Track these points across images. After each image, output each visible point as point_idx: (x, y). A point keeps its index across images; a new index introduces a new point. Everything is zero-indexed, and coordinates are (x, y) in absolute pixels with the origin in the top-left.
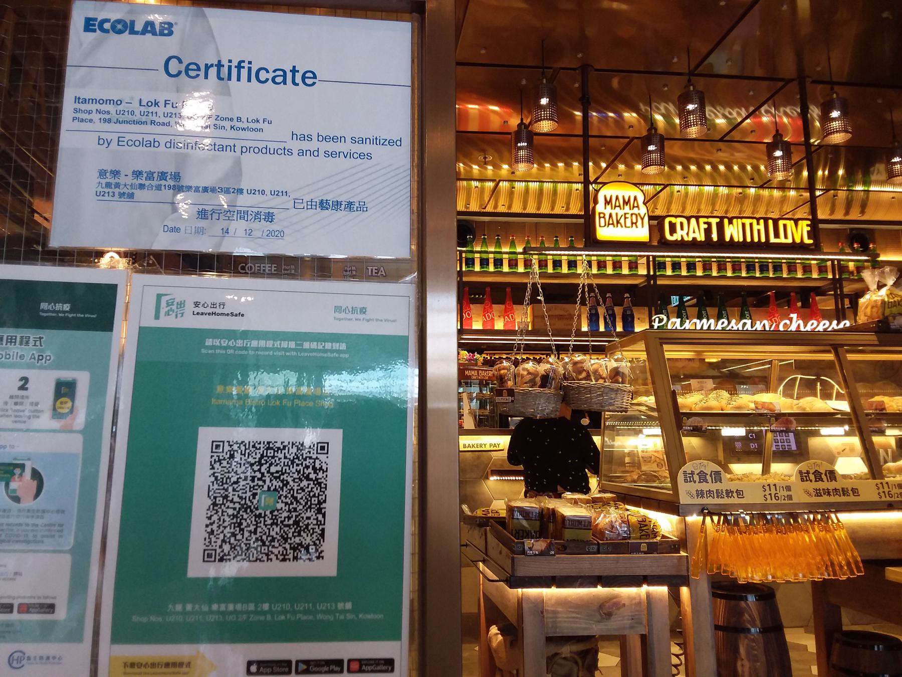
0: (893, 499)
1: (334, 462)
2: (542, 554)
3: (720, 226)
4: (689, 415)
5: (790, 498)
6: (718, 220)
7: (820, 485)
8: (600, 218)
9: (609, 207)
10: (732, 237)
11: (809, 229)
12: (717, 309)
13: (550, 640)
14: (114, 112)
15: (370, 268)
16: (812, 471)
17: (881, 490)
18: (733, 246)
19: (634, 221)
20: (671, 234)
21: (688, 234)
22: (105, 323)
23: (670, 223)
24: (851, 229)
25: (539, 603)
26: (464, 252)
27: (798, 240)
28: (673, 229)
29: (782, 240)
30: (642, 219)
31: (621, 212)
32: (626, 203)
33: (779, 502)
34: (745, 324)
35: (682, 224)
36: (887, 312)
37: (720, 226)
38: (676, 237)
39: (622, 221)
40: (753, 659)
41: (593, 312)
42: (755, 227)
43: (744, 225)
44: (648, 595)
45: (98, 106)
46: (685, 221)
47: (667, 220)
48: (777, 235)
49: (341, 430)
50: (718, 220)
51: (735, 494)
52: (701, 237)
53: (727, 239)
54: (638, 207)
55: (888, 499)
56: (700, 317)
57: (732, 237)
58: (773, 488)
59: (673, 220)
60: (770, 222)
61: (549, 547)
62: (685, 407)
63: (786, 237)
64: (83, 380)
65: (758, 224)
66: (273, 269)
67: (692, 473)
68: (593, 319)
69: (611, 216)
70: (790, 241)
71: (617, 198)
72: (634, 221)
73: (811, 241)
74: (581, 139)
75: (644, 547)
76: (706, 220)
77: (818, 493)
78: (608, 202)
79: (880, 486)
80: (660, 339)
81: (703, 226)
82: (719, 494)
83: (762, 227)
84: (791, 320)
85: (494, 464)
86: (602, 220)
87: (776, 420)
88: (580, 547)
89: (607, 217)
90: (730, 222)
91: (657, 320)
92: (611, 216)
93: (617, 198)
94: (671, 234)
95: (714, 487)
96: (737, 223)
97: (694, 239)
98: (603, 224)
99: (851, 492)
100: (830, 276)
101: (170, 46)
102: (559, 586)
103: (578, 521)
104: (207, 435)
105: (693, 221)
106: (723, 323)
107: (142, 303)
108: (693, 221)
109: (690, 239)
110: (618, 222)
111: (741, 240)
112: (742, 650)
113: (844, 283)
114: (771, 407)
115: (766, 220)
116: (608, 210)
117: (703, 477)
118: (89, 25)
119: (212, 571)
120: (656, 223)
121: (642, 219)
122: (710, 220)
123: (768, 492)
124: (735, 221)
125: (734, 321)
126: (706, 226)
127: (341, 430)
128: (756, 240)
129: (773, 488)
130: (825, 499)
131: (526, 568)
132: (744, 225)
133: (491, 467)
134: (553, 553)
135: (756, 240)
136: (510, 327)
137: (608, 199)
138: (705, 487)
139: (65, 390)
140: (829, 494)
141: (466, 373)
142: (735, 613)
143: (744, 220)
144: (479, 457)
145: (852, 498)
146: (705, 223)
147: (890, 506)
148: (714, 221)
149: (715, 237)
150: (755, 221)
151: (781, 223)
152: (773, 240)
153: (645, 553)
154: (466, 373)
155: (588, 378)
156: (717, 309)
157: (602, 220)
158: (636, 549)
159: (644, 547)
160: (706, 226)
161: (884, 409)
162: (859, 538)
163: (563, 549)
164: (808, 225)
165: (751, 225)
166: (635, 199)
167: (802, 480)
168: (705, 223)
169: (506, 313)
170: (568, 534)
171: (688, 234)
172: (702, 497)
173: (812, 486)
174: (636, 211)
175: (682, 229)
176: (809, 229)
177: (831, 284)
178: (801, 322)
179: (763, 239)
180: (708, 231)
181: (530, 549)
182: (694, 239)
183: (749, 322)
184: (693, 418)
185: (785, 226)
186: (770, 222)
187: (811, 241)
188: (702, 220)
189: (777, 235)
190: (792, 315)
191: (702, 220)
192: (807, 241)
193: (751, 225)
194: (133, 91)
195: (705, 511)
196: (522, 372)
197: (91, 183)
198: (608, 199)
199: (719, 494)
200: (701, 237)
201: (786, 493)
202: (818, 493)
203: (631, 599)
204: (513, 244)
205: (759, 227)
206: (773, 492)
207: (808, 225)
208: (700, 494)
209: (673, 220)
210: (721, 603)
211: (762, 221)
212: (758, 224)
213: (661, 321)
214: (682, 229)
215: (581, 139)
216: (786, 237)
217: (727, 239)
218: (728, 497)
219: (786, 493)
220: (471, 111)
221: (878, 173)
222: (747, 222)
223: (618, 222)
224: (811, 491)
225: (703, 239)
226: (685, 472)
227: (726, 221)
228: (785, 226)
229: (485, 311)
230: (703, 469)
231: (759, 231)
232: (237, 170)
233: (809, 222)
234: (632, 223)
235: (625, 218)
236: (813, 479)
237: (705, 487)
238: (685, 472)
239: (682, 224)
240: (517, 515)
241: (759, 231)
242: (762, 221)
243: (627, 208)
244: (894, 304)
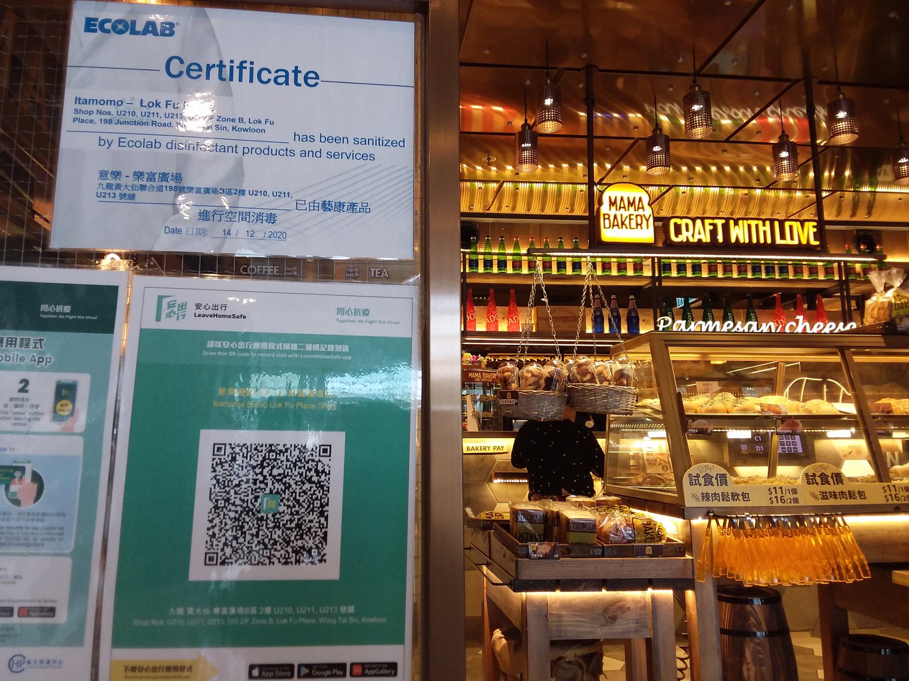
0: (900, 502)
1: (336, 465)
2: (546, 557)
3: (726, 228)
4: (695, 418)
5: (796, 501)
6: (724, 221)
7: (826, 488)
8: (605, 219)
9: (613, 208)
10: (737, 239)
11: (815, 230)
12: (722, 311)
13: (554, 644)
14: (115, 112)
15: (373, 270)
16: (818, 474)
17: (888, 493)
18: (738, 247)
19: (639, 222)
20: (677, 236)
21: (693, 235)
22: (106, 325)
23: (675, 224)
24: (858, 231)
25: (543, 607)
26: (468, 253)
27: (804, 242)
28: (678, 231)
29: (788, 241)
30: (647, 220)
31: (625, 214)
32: (631, 204)
33: (785, 505)
34: (750, 326)
35: (687, 225)
36: (894, 314)
37: (726, 228)
38: (682, 238)
39: (627, 222)
40: (759, 663)
41: (598, 313)
42: (761, 229)
43: (749, 226)
44: (653, 599)
45: (99, 107)
46: (690, 222)
47: (672, 222)
48: (783, 237)
49: (344, 433)
50: (724, 221)
51: (741, 497)
52: (706, 239)
53: (733, 240)
54: (643, 208)
55: (895, 502)
56: (705, 319)
57: (737, 239)
58: (779, 491)
59: (678, 221)
60: (776, 224)
61: (553, 551)
62: (690, 409)
63: (792, 238)
64: (84, 382)
65: (764, 225)
66: (275, 270)
67: (698, 476)
68: (598, 321)
69: (615, 217)
70: (796, 242)
71: (622, 199)
72: (639, 222)
73: (817, 243)
74: (585, 140)
75: (649, 551)
76: (711, 221)
77: (824, 496)
78: (612, 203)
79: (887, 489)
80: (665, 341)
81: (709, 228)
82: (724, 497)
83: (768, 228)
84: (797, 322)
85: (498, 467)
86: (607, 221)
87: (782, 422)
88: (584, 550)
89: (612, 218)
90: (736, 224)
91: (662, 322)
92: (615, 217)
93: (622, 199)
94: (677, 236)
95: (719, 490)
96: (743, 224)
97: (700, 240)
98: (607, 225)
99: (857, 495)
100: (837, 278)
101: (171, 46)
102: (563, 589)
103: (583, 524)
104: (208, 438)
105: (699, 222)
106: (729, 325)
107: (143, 304)
108: (699, 222)
109: (696, 240)
110: (623, 223)
111: (747, 241)
112: (748, 654)
113: (851, 285)
114: (777, 409)
115: (772, 221)
116: (613, 212)
117: (708, 480)
118: (90, 26)
119: (214, 574)
120: (662, 224)
121: (647, 220)
122: (716, 221)
123: (774, 495)
124: (740, 222)
125: (739, 323)
126: (711, 227)
127: (344, 433)
128: (762, 241)
129: (779, 491)
130: (831, 502)
131: (530, 571)
132: (749, 226)
133: (494, 470)
134: (557, 556)
135: (762, 241)
136: (514, 329)
137: (613, 201)
138: (710, 490)
139: (65, 392)
140: (835, 497)
141: (470, 375)
142: (741, 616)
143: (750, 222)
144: (482, 460)
145: (858, 501)
146: (710, 224)
147: (897, 509)
148: (720, 223)
149: (720, 238)
150: (760, 223)
151: (787, 224)
152: (779, 241)
153: (650, 556)
154: (470, 375)
155: (592, 380)
156: (722, 311)
157: (607, 221)
158: (641, 552)
159: (649, 551)
160: (711, 227)
161: (891, 411)
162: (866, 541)
163: (567, 552)
164: (814, 227)
165: (757, 226)
166: (640, 200)
167: (809, 483)
168: (710, 224)
169: (510, 315)
170: (573, 537)
171: (693, 235)
172: (708, 500)
173: (818, 489)
174: (641, 212)
175: (687, 230)
176: (815, 230)
177: (838, 285)
178: (807, 324)
179: (769, 241)
180: (714, 233)
181: (535, 552)
182: (700, 240)
183: (754, 324)
184: (699, 421)
185: (791, 227)
186: (776, 224)
187: (817, 243)
188: (707, 222)
189: (783, 237)
190: (798, 317)
191: (707, 222)
192: (814, 242)
193: (757, 226)
194: (134, 92)
195: (710, 514)
196: (526, 374)
197: (92, 184)
198: (613, 201)
199: (724, 497)
200: (706, 239)
201: (792, 496)
202: (824, 496)
203: (636, 602)
204: (517, 246)
205: (764, 228)
206: (779, 495)
207: (814, 227)
208: (706, 496)
209: (678, 221)
210: (727, 607)
211: (768, 223)
212: (764, 225)
213: (666, 322)
214: (687, 230)
215: (585, 140)
216: (792, 238)
217: (733, 240)
218: (733, 500)
219: (792, 496)
220: (475, 112)
221: (885, 174)
222: (753, 223)
223: (623, 223)
224: (818, 494)
225: (709, 241)
226: (690, 475)
227: (732, 222)
228: (791, 227)
229: (489, 313)
230: (708, 472)
231: (765, 232)
232: (238, 171)
233: (815, 224)
234: (637, 225)
235: (630, 219)
236: (820, 482)
237: (710, 490)
238: (690, 475)
239: (687, 225)
240: (521, 518)
241: (765, 232)
242: (768, 223)
243: (632, 209)
244: (901, 306)
